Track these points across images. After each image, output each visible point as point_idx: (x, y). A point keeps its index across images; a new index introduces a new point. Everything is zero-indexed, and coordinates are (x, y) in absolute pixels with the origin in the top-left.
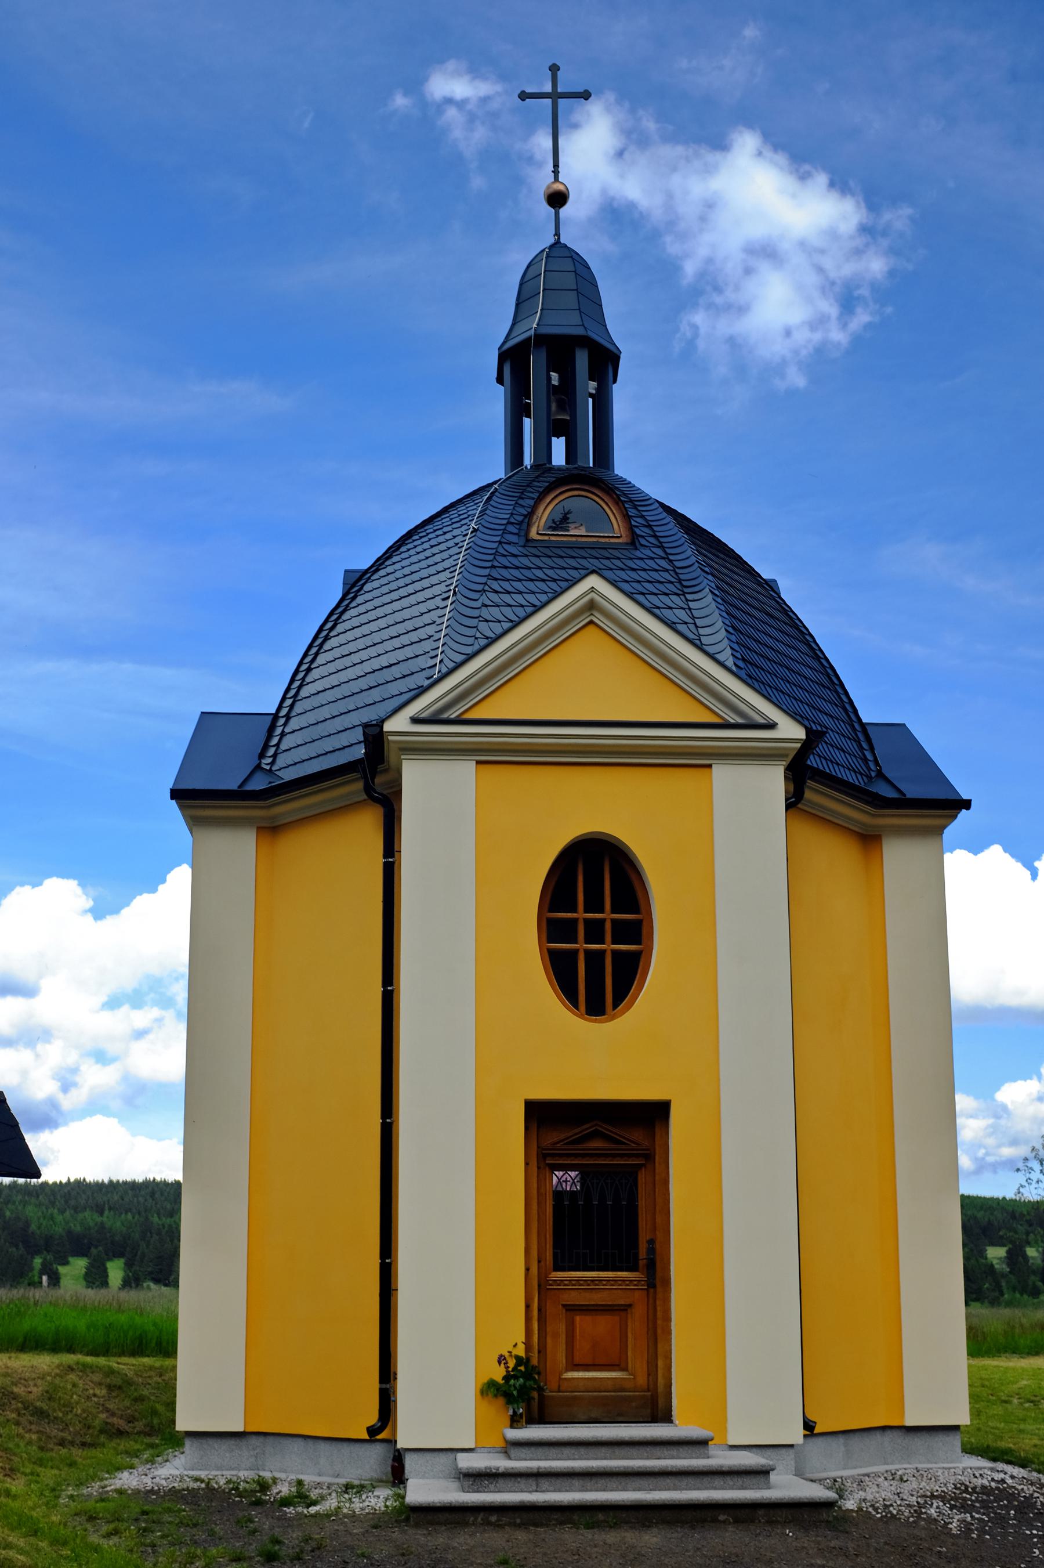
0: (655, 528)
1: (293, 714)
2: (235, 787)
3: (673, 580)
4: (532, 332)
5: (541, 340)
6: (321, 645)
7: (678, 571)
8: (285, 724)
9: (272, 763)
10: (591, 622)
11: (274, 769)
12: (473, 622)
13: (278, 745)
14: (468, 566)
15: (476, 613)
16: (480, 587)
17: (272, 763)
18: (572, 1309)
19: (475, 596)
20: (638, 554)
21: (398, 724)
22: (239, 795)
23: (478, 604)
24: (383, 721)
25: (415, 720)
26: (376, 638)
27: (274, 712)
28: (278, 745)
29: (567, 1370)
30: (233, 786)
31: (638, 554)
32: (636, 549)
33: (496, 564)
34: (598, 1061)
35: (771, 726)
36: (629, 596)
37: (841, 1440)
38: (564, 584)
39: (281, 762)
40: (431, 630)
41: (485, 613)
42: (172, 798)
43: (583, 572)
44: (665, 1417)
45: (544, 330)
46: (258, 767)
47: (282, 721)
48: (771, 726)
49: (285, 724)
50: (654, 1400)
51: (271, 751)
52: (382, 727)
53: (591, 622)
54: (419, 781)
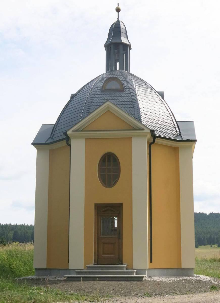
0: (129, 87)
1: (57, 126)
2: (44, 143)
3: (131, 98)
4: (110, 42)
5: (112, 43)
6: (63, 112)
7: (132, 96)
8: (55, 129)
9: (53, 137)
10: (108, 110)
11: (53, 138)
12: (88, 110)
13: (54, 133)
14: (89, 98)
15: (89, 107)
16: (90, 102)
17: (53, 137)
18: (104, 243)
19: (89, 104)
20: (124, 93)
21: (69, 132)
22: (45, 144)
23: (90, 106)
24: (67, 132)
25: (73, 131)
26: (73, 111)
27: (55, 124)
28: (54, 133)
29: (103, 255)
30: (44, 142)
31: (124, 93)
32: (124, 92)
33: (95, 97)
34: (109, 196)
35: (143, 129)
36: (116, 105)
37: (165, 270)
38: (93, 110)
39: (54, 136)
40: (80, 111)
41: (91, 108)
42: (32, 145)
43: (106, 101)
44: (122, 264)
45: (112, 42)
46: (50, 137)
47: (55, 128)
48: (143, 129)
49: (55, 129)
50: (120, 260)
51: (53, 134)
52: (66, 133)
53: (108, 110)
54: (73, 143)
